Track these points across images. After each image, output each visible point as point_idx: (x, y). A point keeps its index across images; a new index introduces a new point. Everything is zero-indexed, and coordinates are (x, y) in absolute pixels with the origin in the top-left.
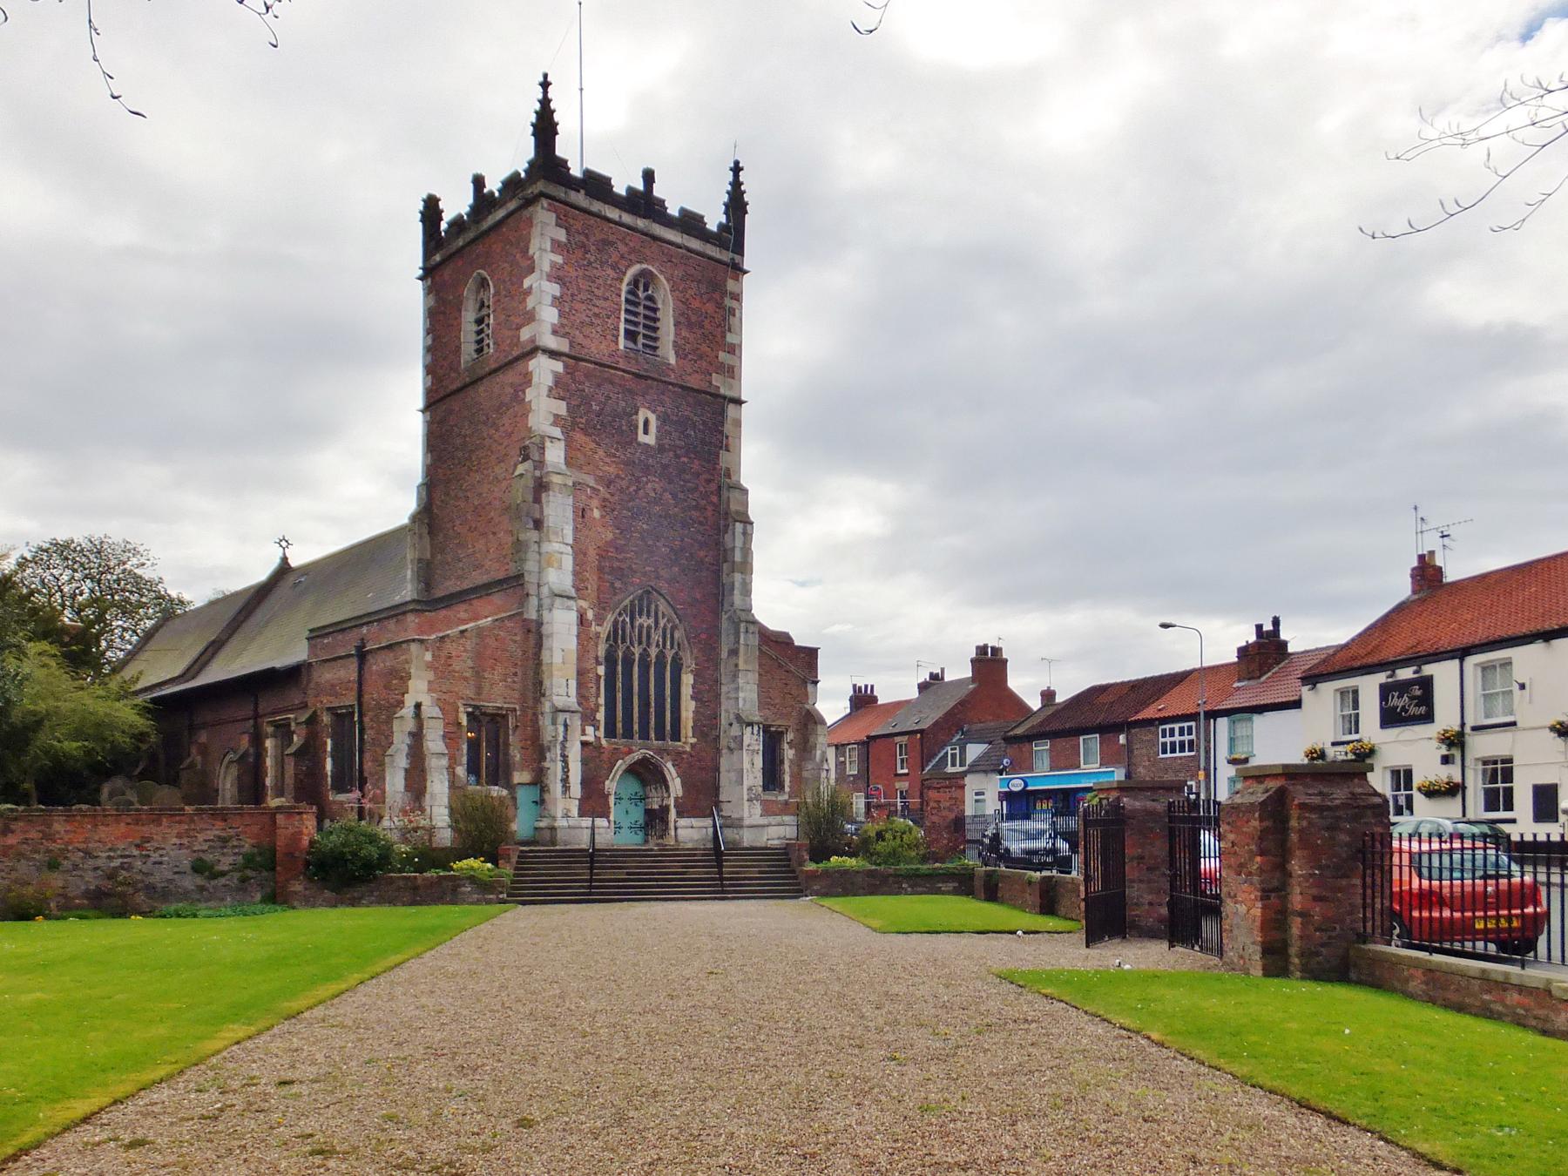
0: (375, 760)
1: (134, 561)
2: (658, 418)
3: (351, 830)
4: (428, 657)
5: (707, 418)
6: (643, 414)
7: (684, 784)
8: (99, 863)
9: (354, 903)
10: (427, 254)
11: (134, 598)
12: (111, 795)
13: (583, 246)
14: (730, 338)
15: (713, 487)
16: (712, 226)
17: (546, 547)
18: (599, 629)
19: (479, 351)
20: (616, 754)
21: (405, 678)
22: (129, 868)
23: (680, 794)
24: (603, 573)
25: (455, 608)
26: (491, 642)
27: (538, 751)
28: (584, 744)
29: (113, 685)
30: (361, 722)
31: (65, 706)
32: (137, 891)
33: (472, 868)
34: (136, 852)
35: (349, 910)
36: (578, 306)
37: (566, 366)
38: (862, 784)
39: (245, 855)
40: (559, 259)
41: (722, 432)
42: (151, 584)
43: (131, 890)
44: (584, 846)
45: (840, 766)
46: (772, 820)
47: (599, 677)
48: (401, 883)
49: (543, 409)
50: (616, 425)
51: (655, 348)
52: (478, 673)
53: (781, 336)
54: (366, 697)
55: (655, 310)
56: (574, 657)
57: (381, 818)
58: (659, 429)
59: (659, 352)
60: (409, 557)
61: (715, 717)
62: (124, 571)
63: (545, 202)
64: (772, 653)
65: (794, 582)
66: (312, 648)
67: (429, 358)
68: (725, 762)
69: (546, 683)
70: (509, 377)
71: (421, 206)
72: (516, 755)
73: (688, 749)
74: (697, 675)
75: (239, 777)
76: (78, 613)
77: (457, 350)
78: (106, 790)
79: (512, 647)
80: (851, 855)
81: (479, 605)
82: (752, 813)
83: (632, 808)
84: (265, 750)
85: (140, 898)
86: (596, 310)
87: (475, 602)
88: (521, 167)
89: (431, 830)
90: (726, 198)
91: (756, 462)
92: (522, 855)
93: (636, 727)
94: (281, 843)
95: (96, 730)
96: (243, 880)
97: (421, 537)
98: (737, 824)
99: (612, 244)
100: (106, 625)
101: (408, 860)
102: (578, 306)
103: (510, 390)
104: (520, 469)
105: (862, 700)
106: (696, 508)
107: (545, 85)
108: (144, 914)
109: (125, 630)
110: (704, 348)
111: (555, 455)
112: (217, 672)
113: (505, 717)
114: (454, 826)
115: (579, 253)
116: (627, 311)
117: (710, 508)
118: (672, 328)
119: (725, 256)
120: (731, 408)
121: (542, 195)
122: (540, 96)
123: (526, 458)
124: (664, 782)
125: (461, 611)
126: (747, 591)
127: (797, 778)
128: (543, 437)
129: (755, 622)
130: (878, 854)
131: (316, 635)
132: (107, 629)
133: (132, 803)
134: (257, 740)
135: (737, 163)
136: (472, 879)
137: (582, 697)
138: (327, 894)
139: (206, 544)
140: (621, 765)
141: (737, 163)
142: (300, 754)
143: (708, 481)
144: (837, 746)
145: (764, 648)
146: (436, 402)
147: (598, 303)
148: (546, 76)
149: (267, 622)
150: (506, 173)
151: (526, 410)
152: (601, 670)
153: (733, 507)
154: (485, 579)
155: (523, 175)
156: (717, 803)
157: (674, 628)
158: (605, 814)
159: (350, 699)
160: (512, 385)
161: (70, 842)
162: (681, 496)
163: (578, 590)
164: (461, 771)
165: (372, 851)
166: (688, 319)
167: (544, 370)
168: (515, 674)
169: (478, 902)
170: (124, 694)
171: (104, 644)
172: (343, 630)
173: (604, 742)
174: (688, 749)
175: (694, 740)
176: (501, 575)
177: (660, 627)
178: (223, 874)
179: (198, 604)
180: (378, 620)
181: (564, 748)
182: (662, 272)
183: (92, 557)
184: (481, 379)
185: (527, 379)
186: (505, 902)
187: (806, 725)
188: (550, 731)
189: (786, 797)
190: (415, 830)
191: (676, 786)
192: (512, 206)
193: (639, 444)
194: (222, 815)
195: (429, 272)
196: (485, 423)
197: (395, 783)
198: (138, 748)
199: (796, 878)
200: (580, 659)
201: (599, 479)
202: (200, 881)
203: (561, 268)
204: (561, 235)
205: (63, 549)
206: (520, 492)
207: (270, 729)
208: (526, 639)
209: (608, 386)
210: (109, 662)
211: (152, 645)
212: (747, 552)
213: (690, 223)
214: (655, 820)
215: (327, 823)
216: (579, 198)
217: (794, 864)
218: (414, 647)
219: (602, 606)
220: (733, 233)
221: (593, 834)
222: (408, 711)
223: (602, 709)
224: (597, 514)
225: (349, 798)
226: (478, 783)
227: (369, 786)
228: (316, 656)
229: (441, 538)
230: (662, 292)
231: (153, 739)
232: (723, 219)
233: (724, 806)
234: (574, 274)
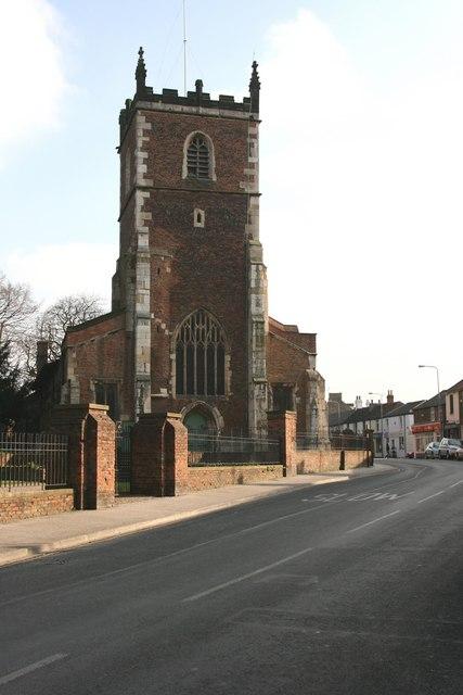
47: (171, 361)
56: (148, 351)
107: (141, 53)
120: (252, 200)
152: (173, 357)
191: (220, 421)
213: (226, 101)
223: (174, 379)
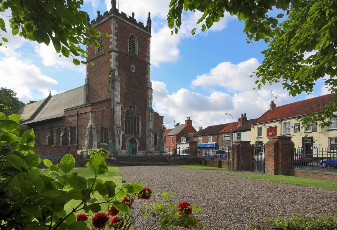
18: (124, 111)
27: (114, 136)
30: (77, 129)
40: (117, 31)
56: (120, 117)
61: (145, 130)
63: (114, 18)
68: (147, 140)
74: (142, 121)
84: (54, 135)
112: (36, 119)
113: (107, 129)
124: (136, 143)
135: (149, 13)
141: (149, 13)
152: (125, 119)
182: (136, 35)
191: (138, 144)
193: (132, 72)
212: (151, 95)
213: (141, 24)
214: (134, 151)
216: (120, 18)
223: (125, 128)
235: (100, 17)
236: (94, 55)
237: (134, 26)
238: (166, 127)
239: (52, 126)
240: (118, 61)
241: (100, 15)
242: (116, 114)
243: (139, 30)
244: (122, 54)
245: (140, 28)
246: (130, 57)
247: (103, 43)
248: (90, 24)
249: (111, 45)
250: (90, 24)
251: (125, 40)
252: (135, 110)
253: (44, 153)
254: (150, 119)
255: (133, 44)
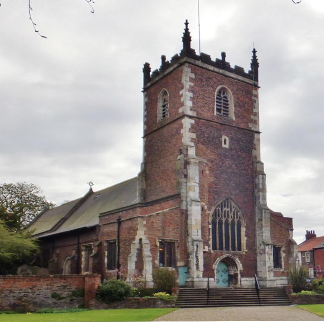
0: (124, 259)
1: (35, 191)
2: (229, 139)
3: (114, 283)
4: (145, 222)
5: (248, 139)
6: (224, 137)
7: (243, 266)
8: (15, 294)
9: (115, 308)
10: (145, 83)
11: (34, 204)
12: (21, 271)
13: (201, 79)
14: (255, 110)
15: (250, 162)
16: (247, 71)
17: (189, 184)
18: (209, 212)
19: (164, 116)
20: (217, 256)
21: (135, 230)
22: (27, 296)
23: (242, 269)
24: (210, 193)
25: (155, 206)
26: (168, 217)
27: (186, 255)
28: (204, 252)
29: (25, 233)
30: (119, 245)
31: (5, 241)
32: (30, 304)
33: (161, 296)
34: (30, 291)
35: (113, 310)
36: (199, 100)
37: (195, 121)
38: (312, 265)
39: (72, 292)
40: (192, 84)
41: (253, 143)
42: (40, 199)
43: (27, 304)
44: (205, 288)
45: (303, 259)
46: (278, 278)
47: (209, 229)
48: (134, 301)
49: (187, 137)
50: (214, 141)
51: (228, 115)
52: (164, 228)
53: (272, 110)
54: (121, 237)
55: (227, 101)
56: (200, 222)
57: (126, 278)
58: (230, 143)
59: (229, 116)
60: (138, 188)
61: (254, 242)
62: (31, 194)
63: (187, 65)
64: (274, 220)
65: (283, 195)
66: (101, 220)
67: (146, 119)
68: (259, 258)
69: (190, 231)
70: (175, 125)
71: (143, 67)
72: (178, 256)
73: (244, 253)
74: (247, 228)
75: (71, 265)
76: (12, 209)
77: (156, 116)
78: (19, 270)
79: (177, 219)
80: (309, 290)
81: (164, 204)
82: (270, 276)
83: (223, 274)
84: (82, 255)
85: (31, 306)
86: (206, 102)
87: (162, 203)
88: (178, 52)
89: (145, 283)
90: (251, 62)
91: (266, 153)
92: (181, 291)
93: (224, 246)
94: (87, 287)
95: (18, 249)
96: (72, 300)
97: (142, 181)
98: (265, 280)
99: (211, 78)
100: (23, 213)
101: (136, 293)
102: (199, 100)
103: (175, 130)
104: (179, 157)
105: (310, 236)
106: (245, 170)
107: (187, 24)
108: (32, 312)
109: (30, 214)
110: (245, 114)
111: (192, 152)
112: (64, 229)
113: (174, 243)
114: (154, 281)
115: (199, 82)
116: (217, 102)
117: (250, 170)
118: (233, 107)
119: (252, 82)
120: (256, 135)
121: (186, 62)
122: (185, 28)
123: (181, 153)
124: (235, 265)
125: (157, 206)
126: (264, 198)
127: (287, 263)
128: (187, 146)
129: (268, 209)
130: (320, 290)
131: (102, 216)
132: (23, 214)
133: (29, 274)
134: (79, 252)
135: (254, 50)
136: (161, 299)
137: (203, 236)
138: (104, 305)
139: (60, 185)
140: (218, 259)
141: (254, 50)
142: (95, 257)
143: (249, 160)
144: (302, 252)
145: (272, 218)
146: (148, 134)
147: (207, 99)
148: (187, 21)
149: (83, 212)
150: (173, 55)
151: (181, 137)
152: (210, 227)
153: (258, 169)
154: (166, 195)
155: (179, 55)
156: (256, 273)
157: (237, 212)
158: (213, 276)
159: (115, 237)
160: (176, 128)
161: (4, 288)
162: (239, 165)
163: (201, 199)
164: (157, 262)
165: (123, 290)
166: (239, 104)
167: (187, 123)
168: (178, 228)
169: (164, 307)
170: (28, 236)
171: (21, 219)
172: (113, 214)
173: (212, 251)
174: (244, 253)
175: (246, 251)
176: (172, 194)
177: (232, 212)
178: (64, 298)
179: (58, 205)
180: (132, 208)
181: (196, 253)
182: (229, 88)
183: (19, 190)
184: (164, 126)
185: (181, 126)
186: (174, 307)
187: (289, 245)
188: (191, 248)
189: (283, 270)
190: (139, 282)
191: (240, 267)
192: (175, 66)
193: (223, 148)
194: (64, 278)
195: (146, 90)
196: (166, 141)
197: (132, 266)
198: (33, 255)
199: (288, 298)
200: (202, 222)
201: (208, 160)
202: (54, 300)
203: (193, 87)
204: (193, 76)
205: (8, 187)
206: (179, 165)
207: (84, 248)
208: (182, 216)
209: (211, 128)
210: (23, 226)
211: (40, 219)
212: (264, 185)
213: (239, 71)
214: (232, 278)
215: (105, 280)
216: (199, 63)
217: (287, 293)
218: (139, 219)
219: (210, 204)
220: (254, 73)
221: (208, 283)
222: (137, 241)
223: (211, 240)
224: (207, 172)
225: (114, 272)
226: (164, 266)
227: (121, 267)
228: (102, 223)
229: (149, 181)
230: (229, 95)
231: (39, 252)
232: (250, 69)
233: (259, 273)
234: (198, 89)
235: (165, 65)
236: (154, 125)
237: (225, 74)
238: (315, 233)
239: (78, 241)
240: (194, 132)
241: (166, 61)
242: (191, 219)
243: (235, 79)
244: (203, 121)
245: (237, 75)
246: (218, 124)
247: (169, 105)
248: (151, 76)
249: (181, 107)
250: (151, 76)
251: (209, 98)
252: (231, 210)
253: (35, 287)
254: (262, 224)
255: (225, 102)
